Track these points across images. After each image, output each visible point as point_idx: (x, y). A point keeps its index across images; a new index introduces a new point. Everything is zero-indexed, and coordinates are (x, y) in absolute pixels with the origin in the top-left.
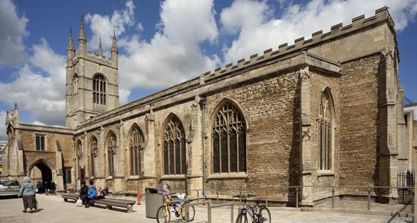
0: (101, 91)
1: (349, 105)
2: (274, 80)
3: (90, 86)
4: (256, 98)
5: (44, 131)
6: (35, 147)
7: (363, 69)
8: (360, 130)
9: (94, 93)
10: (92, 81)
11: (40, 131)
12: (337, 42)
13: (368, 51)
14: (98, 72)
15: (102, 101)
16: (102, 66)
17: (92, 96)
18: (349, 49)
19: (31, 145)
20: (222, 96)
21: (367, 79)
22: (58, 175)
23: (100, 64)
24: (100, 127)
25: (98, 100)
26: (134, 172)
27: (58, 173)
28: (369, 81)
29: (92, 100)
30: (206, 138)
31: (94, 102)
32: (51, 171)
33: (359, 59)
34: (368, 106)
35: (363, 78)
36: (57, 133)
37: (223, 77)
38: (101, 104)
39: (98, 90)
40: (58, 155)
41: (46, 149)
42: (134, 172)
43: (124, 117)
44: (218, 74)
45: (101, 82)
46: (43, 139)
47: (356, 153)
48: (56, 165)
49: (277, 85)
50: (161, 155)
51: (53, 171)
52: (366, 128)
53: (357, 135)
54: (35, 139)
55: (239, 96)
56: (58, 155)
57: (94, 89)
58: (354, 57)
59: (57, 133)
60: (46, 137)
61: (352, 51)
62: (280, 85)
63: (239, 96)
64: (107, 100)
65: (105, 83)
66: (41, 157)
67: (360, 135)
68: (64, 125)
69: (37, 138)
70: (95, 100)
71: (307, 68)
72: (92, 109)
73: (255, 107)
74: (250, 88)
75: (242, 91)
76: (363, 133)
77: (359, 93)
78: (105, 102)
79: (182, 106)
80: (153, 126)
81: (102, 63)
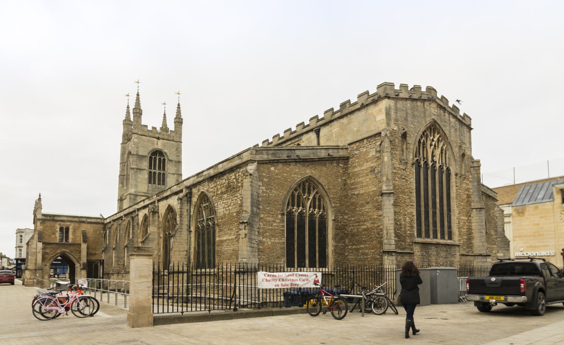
0: (159, 169)
1: (356, 193)
2: (232, 176)
3: (145, 164)
4: (222, 193)
5: (69, 221)
7: (366, 151)
8: (365, 221)
12: (345, 120)
13: (372, 131)
14: (156, 147)
15: (159, 180)
16: (161, 140)
18: (355, 129)
19: (53, 236)
21: (370, 163)
22: (81, 269)
23: (158, 138)
24: (122, 217)
26: (431, 233)
27: (82, 267)
28: (372, 165)
29: (147, 181)
30: (190, 232)
31: (150, 182)
32: (74, 265)
33: (362, 140)
34: (371, 194)
35: (367, 162)
36: (84, 222)
40: (84, 246)
41: (70, 241)
42: (431, 233)
45: (160, 159)
46: (67, 229)
47: (362, 248)
48: (80, 258)
49: (234, 180)
50: (162, 249)
51: (77, 265)
52: (370, 219)
53: (363, 227)
55: (212, 190)
56: (84, 246)
58: (360, 138)
59: (84, 222)
60: (71, 227)
61: (358, 131)
62: (237, 180)
63: (212, 190)
65: (164, 159)
66: (63, 250)
67: (365, 227)
69: (61, 229)
70: (152, 179)
72: (145, 191)
73: (221, 203)
74: (218, 183)
75: (213, 186)
76: (368, 225)
77: (364, 178)
80: (157, 217)
81: (160, 136)
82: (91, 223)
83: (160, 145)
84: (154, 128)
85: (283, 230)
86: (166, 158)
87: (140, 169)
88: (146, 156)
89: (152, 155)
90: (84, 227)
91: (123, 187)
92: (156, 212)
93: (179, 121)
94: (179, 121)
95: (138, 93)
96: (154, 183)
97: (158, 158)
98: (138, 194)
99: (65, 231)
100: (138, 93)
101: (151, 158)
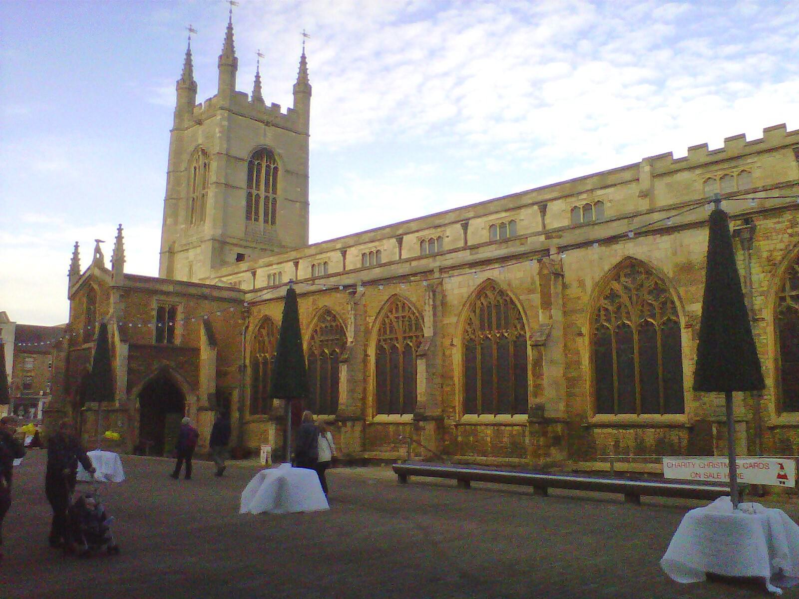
0: (267, 191)
6: (154, 337)
9: (250, 195)
10: (246, 164)
11: (168, 294)
15: (266, 214)
17: (244, 203)
20: (392, 290)
23: (267, 124)
25: (257, 213)
29: (243, 213)
31: (248, 218)
36: (205, 297)
37: (520, 494)
38: (266, 221)
39: (258, 188)
40: (206, 355)
41: (178, 341)
43: (449, 263)
44: (599, 503)
51: (191, 399)
54: (154, 313)
57: (250, 186)
59: (205, 297)
60: (180, 309)
64: (280, 213)
65: (276, 169)
68: (461, 224)
69: (161, 310)
70: (251, 211)
71: (262, 330)
78: (274, 217)
79: (665, 243)
82: (223, 300)
83: (268, 138)
84: (276, 106)
85: (155, 460)
86: (280, 167)
87: (232, 187)
88: (243, 160)
89: (253, 157)
90: (206, 309)
91: (176, 223)
92: (559, 274)
93: (303, 90)
94: (303, 90)
95: (303, 54)
96: (256, 220)
97: (264, 165)
98: (228, 240)
99: (167, 315)
100: (303, 54)
101: (251, 163)
